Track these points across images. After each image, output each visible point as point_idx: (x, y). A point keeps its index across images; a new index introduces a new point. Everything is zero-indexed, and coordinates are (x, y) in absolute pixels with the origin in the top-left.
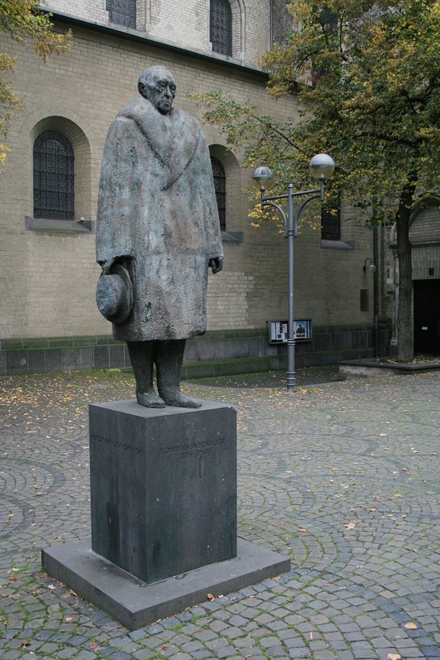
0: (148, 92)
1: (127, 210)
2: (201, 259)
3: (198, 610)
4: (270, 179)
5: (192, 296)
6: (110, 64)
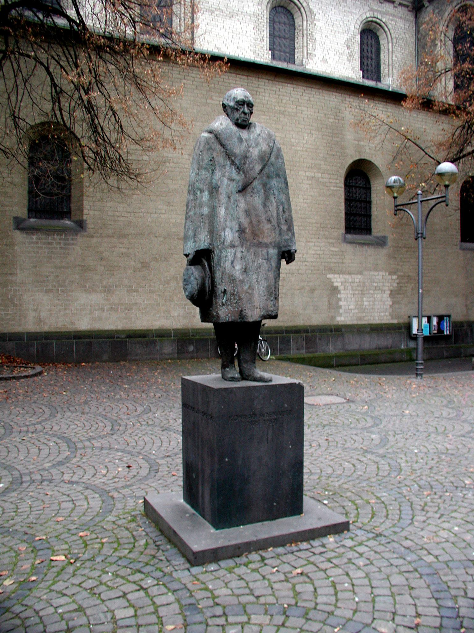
0: (229, 111)
1: (206, 210)
2: (273, 252)
3: (254, 556)
4: (401, 187)
5: (263, 284)
6: (267, 95)
